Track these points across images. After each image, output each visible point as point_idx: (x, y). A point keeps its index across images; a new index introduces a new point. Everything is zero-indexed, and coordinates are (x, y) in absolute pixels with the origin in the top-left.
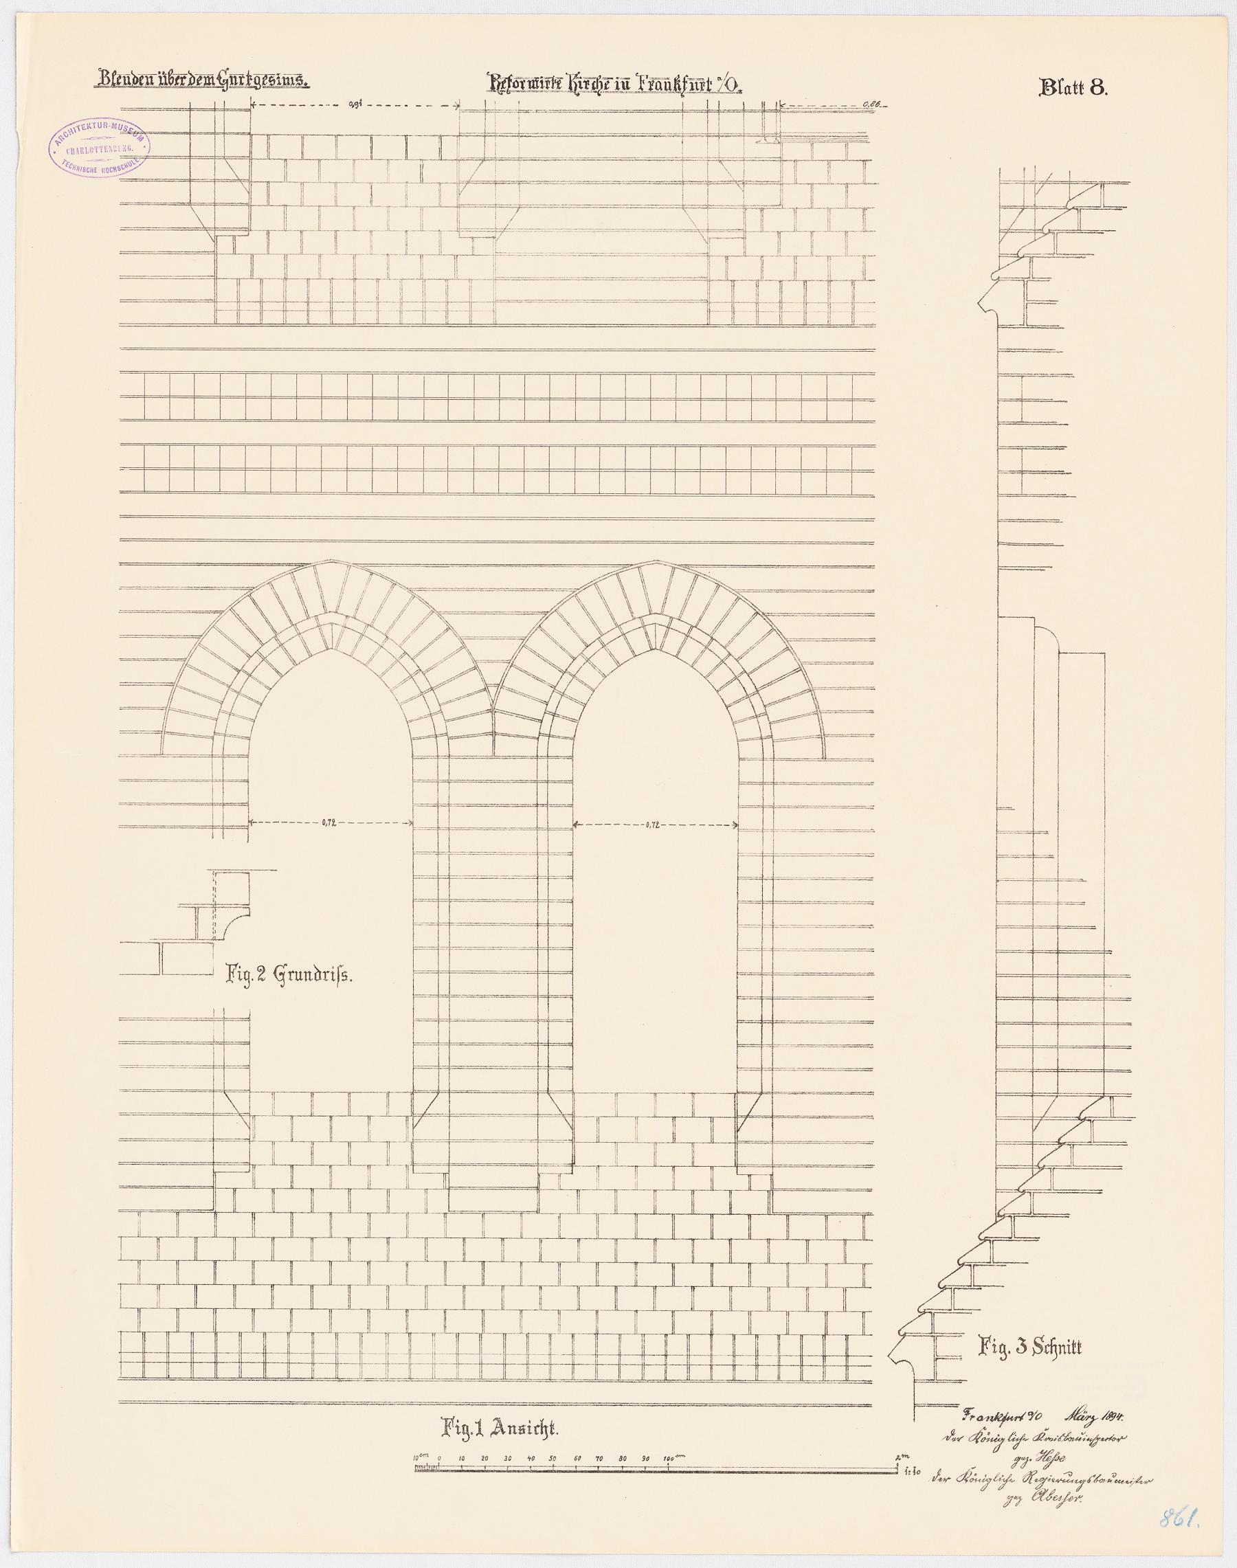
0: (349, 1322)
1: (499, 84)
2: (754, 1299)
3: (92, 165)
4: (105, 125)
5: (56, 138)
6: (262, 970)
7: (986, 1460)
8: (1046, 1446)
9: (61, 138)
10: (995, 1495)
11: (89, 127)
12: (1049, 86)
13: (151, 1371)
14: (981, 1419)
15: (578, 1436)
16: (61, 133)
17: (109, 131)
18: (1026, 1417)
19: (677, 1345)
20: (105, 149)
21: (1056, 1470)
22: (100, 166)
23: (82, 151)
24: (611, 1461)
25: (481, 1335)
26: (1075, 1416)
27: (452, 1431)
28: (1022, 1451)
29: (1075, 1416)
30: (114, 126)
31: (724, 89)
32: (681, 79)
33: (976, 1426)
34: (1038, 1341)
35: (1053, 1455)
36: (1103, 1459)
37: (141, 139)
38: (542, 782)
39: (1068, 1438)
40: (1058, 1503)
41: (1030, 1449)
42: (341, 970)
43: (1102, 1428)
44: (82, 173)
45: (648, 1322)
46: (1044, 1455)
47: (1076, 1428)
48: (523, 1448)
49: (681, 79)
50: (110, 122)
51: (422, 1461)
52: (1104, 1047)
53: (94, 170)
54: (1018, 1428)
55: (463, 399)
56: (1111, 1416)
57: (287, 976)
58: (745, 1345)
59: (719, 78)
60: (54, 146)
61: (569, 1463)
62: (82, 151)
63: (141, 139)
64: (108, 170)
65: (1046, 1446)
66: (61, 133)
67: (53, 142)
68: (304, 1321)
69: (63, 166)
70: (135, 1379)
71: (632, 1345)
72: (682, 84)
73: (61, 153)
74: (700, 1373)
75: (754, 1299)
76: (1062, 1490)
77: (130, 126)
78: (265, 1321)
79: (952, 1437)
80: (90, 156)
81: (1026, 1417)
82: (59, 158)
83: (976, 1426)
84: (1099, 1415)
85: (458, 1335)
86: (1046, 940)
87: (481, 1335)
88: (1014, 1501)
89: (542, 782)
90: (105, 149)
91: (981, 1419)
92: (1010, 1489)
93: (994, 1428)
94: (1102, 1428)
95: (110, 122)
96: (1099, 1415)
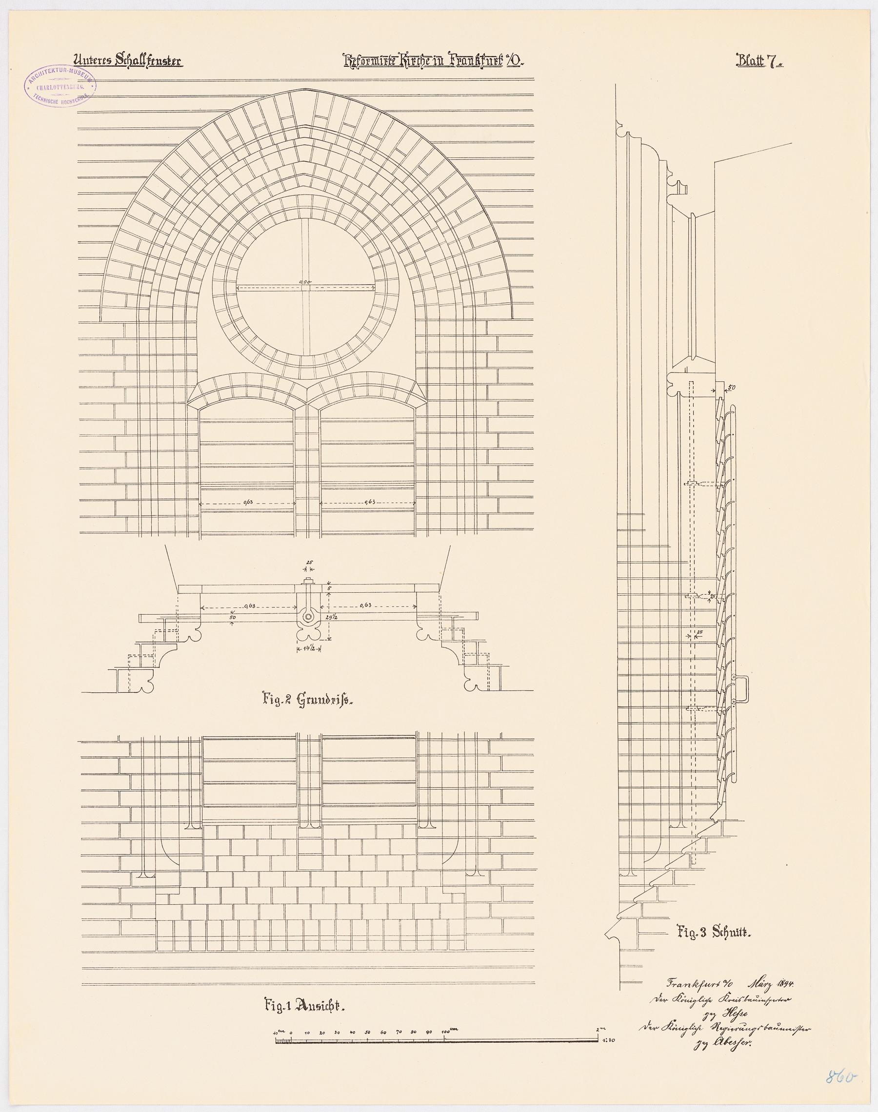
0: (375, 912)
1: (352, 62)
3: (54, 98)
4: (65, 70)
5: (30, 78)
6: (289, 697)
7: (687, 1016)
8: (732, 1005)
9: (33, 78)
10: (691, 1040)
11: (53, 71)
12: (745, 62)
14: (680, 985)
16: (33, 75)
18: (722, 984)
22: (60, 99)
23: (48, 88)
25: (255, 921)
26: (757, 984)
27: (270, 1007)
28: (709, 1008)
29: (757, 984)
31: (511, 64)
33: (677, 991)
34: (716, 927)
39: (747, 999)
40: (733, 1046)
41: (720, 1009)
42: (345, 696)
43: (776, 992)
44: (47, 104)
46: (730, 1011)
51: (280, 1036)
52: (643, 755)
53: (56, 102)
54: (706, 992)
55: (169, 757)
56: (782, 983)
59: (508, 56)
60: (28, 84)
62: (48, 88)
64: (66, 102)
67: (28, 82)
68: (346, 912)
69: (34, 98)
73: (33, 90)
76: (736, 1036)
78: (319, 912)
79: (660, 999)
82: (31, 92)
83: (677, 991)
84: (775, 982)
85: (319, 921)
87: (255, 921)
88: (702, 1046)
91: (680, 985)
92: (700, 1036)
93: (691, 993)
94: (776, 992)
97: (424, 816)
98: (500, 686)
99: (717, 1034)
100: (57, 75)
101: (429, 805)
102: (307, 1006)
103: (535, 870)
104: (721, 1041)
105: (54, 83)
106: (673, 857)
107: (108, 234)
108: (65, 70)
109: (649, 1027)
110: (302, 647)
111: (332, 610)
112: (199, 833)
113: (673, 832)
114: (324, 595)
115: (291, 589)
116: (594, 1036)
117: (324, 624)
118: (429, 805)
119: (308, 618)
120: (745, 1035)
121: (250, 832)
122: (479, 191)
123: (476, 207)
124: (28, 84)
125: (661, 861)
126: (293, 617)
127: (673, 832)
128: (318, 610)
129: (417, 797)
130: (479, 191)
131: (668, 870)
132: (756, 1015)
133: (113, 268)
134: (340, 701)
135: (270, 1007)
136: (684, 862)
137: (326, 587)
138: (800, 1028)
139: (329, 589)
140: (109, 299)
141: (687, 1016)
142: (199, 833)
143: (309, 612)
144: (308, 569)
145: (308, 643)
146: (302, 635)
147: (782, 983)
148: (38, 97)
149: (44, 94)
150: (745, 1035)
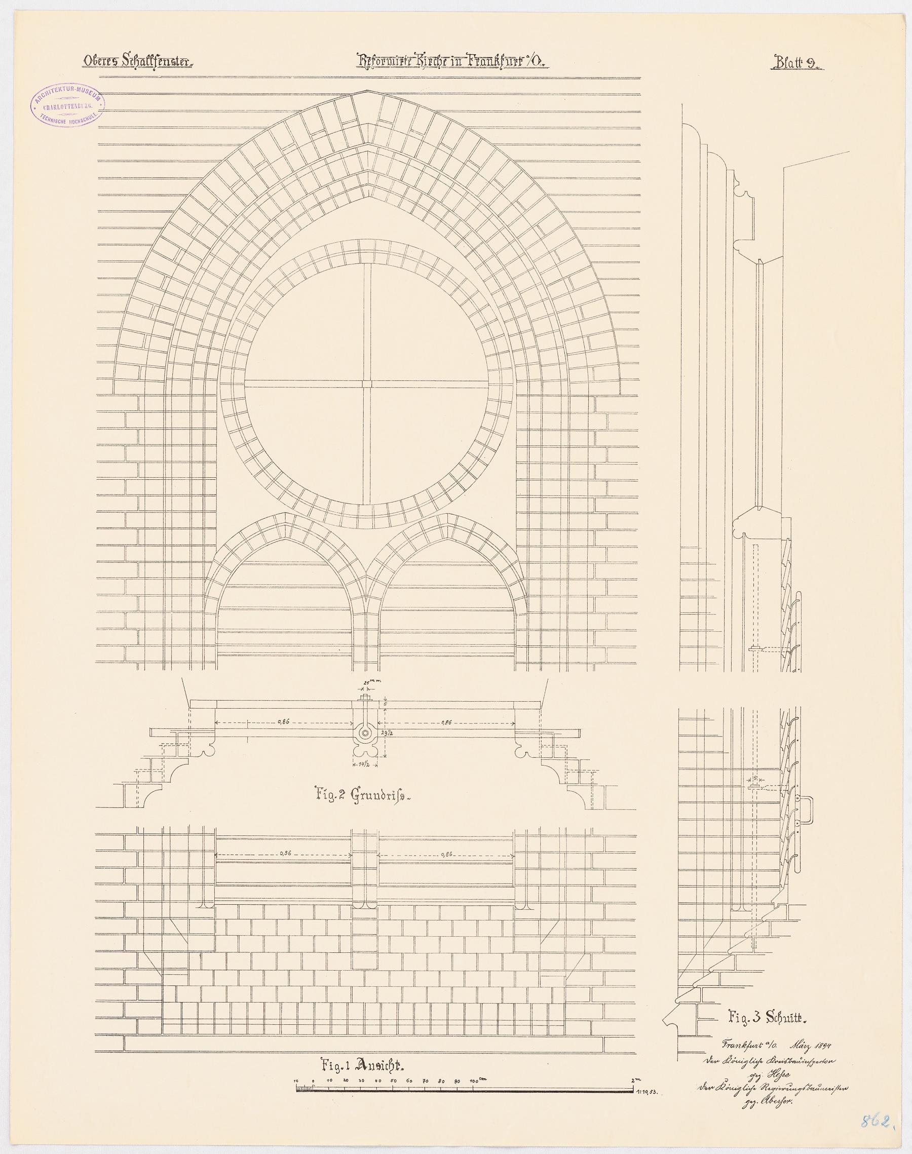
1: (366, 60)
2: (480, 979)
3: (62, 118)
4: (72, 88)
5: (36, 98)
7: (739, 1076)
8: (775, 1066)
12: (781, 64)
13: (537, 1031)
15: (415, 1070)
16: (40, 94)
17: (74, 93)
18: (765, 1046)
19: (356, 1012)
20: (72, 106)
21: (783, 1082)
22: (68, 119)
24: (449, 1084)
27: (327, 1067)
30: (78, 89)
31: (531, 65)
32: (500, 57)
35: (781, 1072)
36: (818, 1075)
37: (98, 99)
38: (700, 736)
39: (791, 1061)
41: (764, 1069)
44: (54, 124)
45: (337, 994)
46: (774, 1072)
47: (797, 1054)
48: (385, 1079)
49: (500, 57)
50: (75, 87)
53: (64, 122)
56: (820, 1046)
57: (360, 797)
58: (422, 1012)
59: (528, 56)
60: (34, 104)
61: (436, 1085)
63: (98, 99)
64: (73, 122)
65: (775, 1066)
66: (40, 94)
70: (458, 1036)
71: (473, 1012)
72: (500, 61)
74: (372, 1029)
75: (480, 979)
76: (779, 1095)
77: (90, 89)
80: (64, 111)
81: (765, 1046)
82: (38, 113)
84: (813, 1045)
86: (197, 553)
88: (755, 1079)
89: (700, 736)
90: (72, 106)
94: (815, 1054)
95: (75, 87)
96: (813, 1045)
97: (521, 897)
98: (214, 1006)
99: (765, 1093)
100: (65, 93)
101: (742, 836)
102: (366, 1065)
103: (761, 971)
104: (768, 1100)
105: (60, 102)
106: (734, 941)
107: (132, 270)
108: (72, 88)
109: (705, 1087)
110: (357, 763)
111: (388, 726)
112: (211, 913)
113: (735, 916)
114: (381, 712)
115: (348, 705)
116: (628, 1086)
117: (381, 740)
118: (742, 836)
119: (365, 733)
120: (790, 1095)
121: (296, 912)
122: (577, 228)
123: (575, 247)
124: (34, 104)
125: (722, 945)
126: (350, 733)
127: (735, 916)
128: (376, 725)
129: (514, 877)
130: (577, 228)
131: (731, 955)
132: (799, 1075)
133: (134, 307)
134: (396, 797)
135: (327, 1067)
136: (746, 945)
137: (382, 703)
138: (839, 1088)
139: (385, 704)
140: (126, 338)
141: (739, 1076)
142: (211, 913)
143: (365, 728)
144: (365, 689)
145: (363, 760)
146: (358, 752)
147: (820, 1046)
148: (45, 117)
149: (52, 114)
150: (790, 1095)
